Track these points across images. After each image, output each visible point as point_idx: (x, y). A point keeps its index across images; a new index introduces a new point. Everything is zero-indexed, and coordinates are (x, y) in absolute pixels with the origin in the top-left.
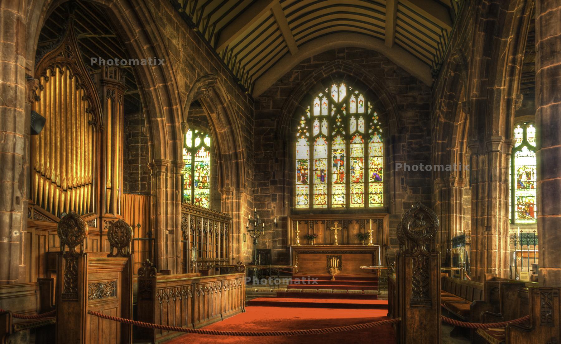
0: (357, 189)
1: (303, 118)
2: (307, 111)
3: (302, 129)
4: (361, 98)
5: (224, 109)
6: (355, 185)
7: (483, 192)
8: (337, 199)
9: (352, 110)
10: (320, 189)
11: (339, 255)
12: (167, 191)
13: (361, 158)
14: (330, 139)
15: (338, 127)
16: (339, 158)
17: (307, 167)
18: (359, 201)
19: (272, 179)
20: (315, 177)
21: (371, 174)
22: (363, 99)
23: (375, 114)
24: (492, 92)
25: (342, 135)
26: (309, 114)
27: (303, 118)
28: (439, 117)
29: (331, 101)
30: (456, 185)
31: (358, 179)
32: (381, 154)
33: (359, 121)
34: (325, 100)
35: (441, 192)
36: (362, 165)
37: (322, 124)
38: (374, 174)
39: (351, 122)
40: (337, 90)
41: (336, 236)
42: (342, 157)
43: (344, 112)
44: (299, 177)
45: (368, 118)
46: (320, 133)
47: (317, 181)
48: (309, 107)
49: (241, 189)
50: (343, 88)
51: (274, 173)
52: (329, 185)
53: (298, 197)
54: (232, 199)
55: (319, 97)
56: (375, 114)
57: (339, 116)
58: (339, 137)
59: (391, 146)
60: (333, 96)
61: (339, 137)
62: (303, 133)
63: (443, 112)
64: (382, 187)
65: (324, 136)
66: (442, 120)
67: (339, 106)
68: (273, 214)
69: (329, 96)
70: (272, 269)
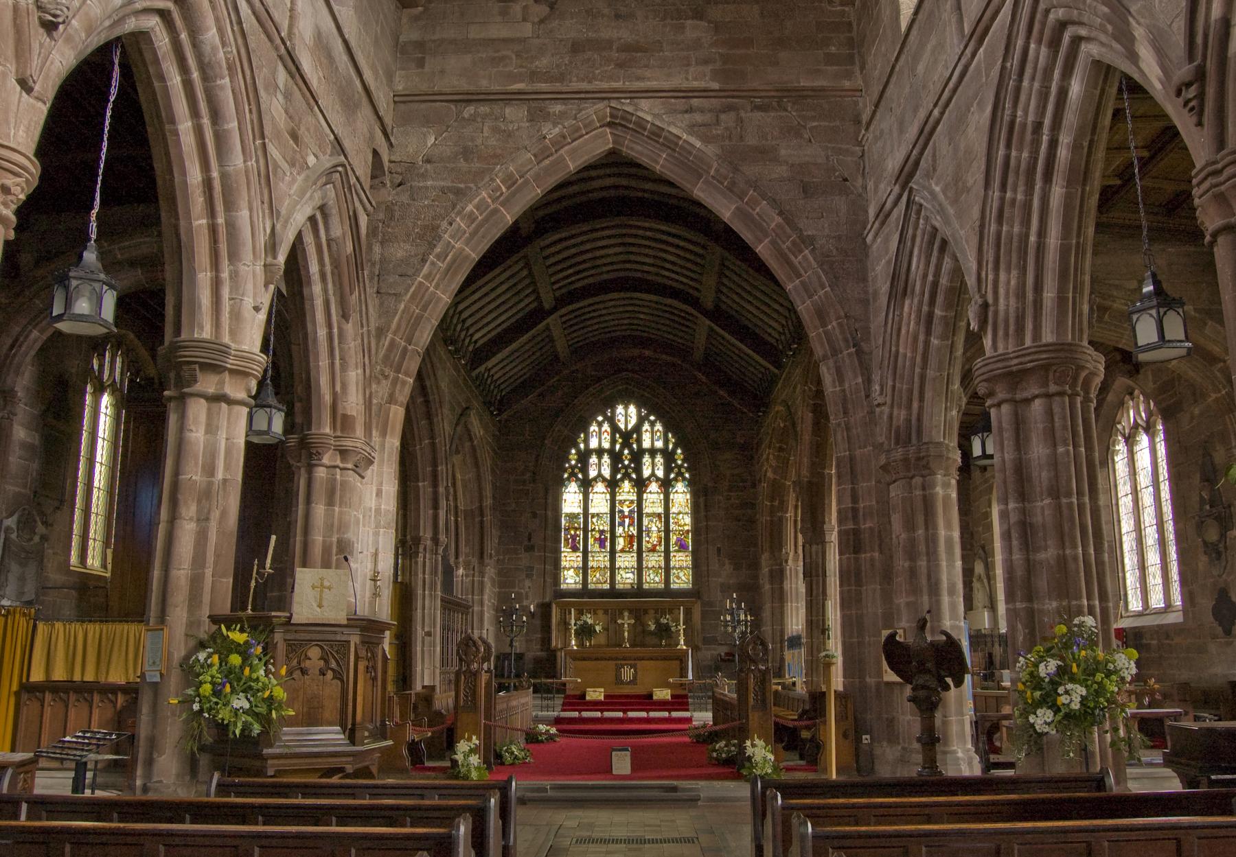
0: (654, 560)
1: (573, 451)
2: (579, 440)
3: (573, 467)
4: (658, 427)
5: (473, 449)
6: (651, 554)
7: (818, 589)
8: (625, 576)
9: (646, 444)
10: (599, 559)
11: (633, 662)
12: (424, 578)
13: (659, 515)
14: (613, 485)
15: (626, 467)
16: (626, 514)
17: (579, 525)
18: (657, 579)
19: (526, 543)
20: (591, 541)
21: (673, 539)
22: (661, 429)
23: (679, 451)
24: (822, 476)
25: (631, 480)
26: (582, 446)
27: (573, 451)
28: (766, 471)
29: (615, 429)
30: (790, 562)
31: (655, 546)
32: (688, 510)
33: (656, 460)
34: (606, 427)
35: (771, 571)
36: (661, 526)
37: (603, 461)
38: (678, 540)
39: (644, 460)
40: (623, 412)
41: (626, 634)
42: (631, 512)
43: (635, 446)
44: (567, 540)
45: (668, 456)
46: (600, 475)
47: (593, 546)
48: (582, 435)
49: (487, 561)
50: (632, 410)
51: (530, 534)
52: (613, 553)
53: (566, 572)
54: (473, 576)
55: (597, 421)
56: (679, 451)
57: (626, 452)
58: (626, 482)
59: (702, 500)
60: (619, 421)
61: (626, 482)
62: (573, 474)
63: (771, 466)
64: (689, 558)
65: (604, 480)
66: (770, 474)
67: (626, 436)
68: (527, 599)
69: (612, 421)
70: (545, 684)
